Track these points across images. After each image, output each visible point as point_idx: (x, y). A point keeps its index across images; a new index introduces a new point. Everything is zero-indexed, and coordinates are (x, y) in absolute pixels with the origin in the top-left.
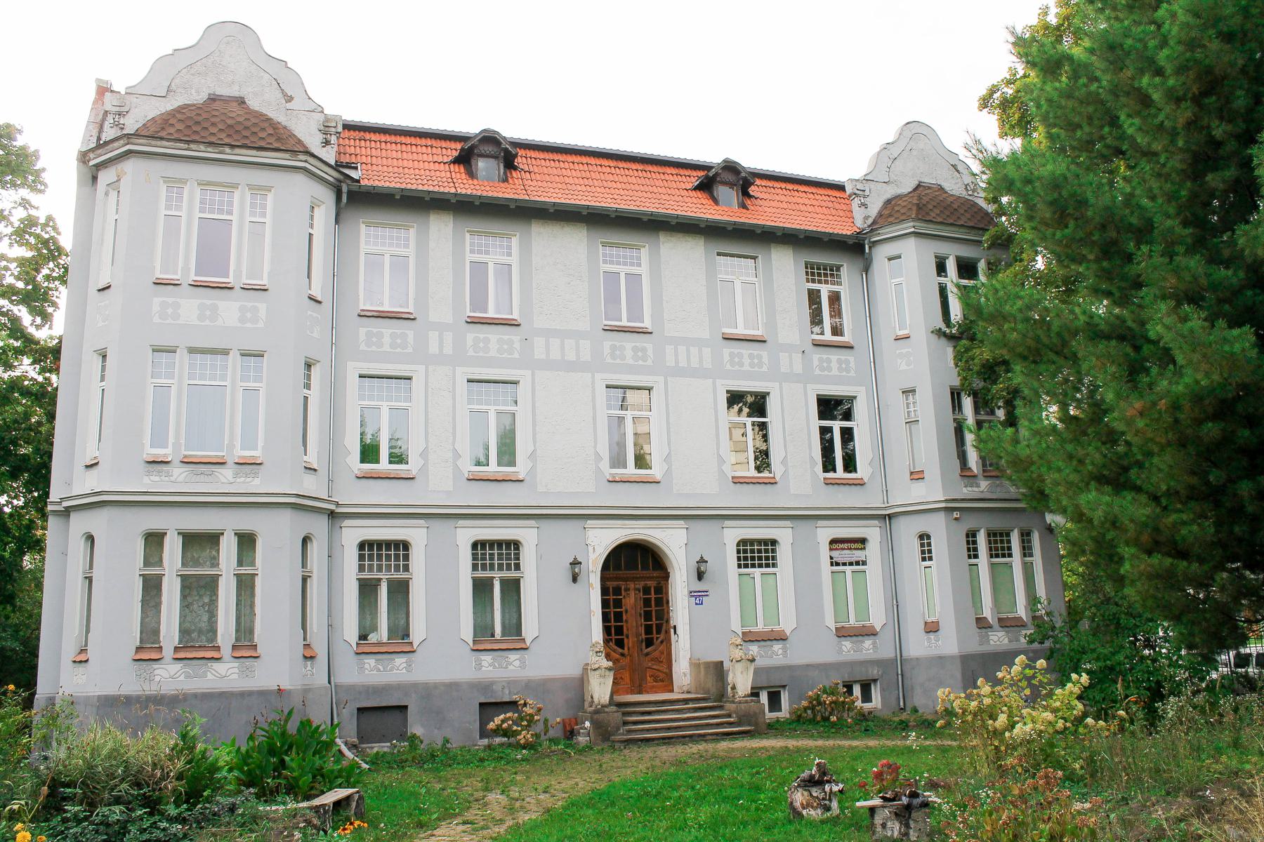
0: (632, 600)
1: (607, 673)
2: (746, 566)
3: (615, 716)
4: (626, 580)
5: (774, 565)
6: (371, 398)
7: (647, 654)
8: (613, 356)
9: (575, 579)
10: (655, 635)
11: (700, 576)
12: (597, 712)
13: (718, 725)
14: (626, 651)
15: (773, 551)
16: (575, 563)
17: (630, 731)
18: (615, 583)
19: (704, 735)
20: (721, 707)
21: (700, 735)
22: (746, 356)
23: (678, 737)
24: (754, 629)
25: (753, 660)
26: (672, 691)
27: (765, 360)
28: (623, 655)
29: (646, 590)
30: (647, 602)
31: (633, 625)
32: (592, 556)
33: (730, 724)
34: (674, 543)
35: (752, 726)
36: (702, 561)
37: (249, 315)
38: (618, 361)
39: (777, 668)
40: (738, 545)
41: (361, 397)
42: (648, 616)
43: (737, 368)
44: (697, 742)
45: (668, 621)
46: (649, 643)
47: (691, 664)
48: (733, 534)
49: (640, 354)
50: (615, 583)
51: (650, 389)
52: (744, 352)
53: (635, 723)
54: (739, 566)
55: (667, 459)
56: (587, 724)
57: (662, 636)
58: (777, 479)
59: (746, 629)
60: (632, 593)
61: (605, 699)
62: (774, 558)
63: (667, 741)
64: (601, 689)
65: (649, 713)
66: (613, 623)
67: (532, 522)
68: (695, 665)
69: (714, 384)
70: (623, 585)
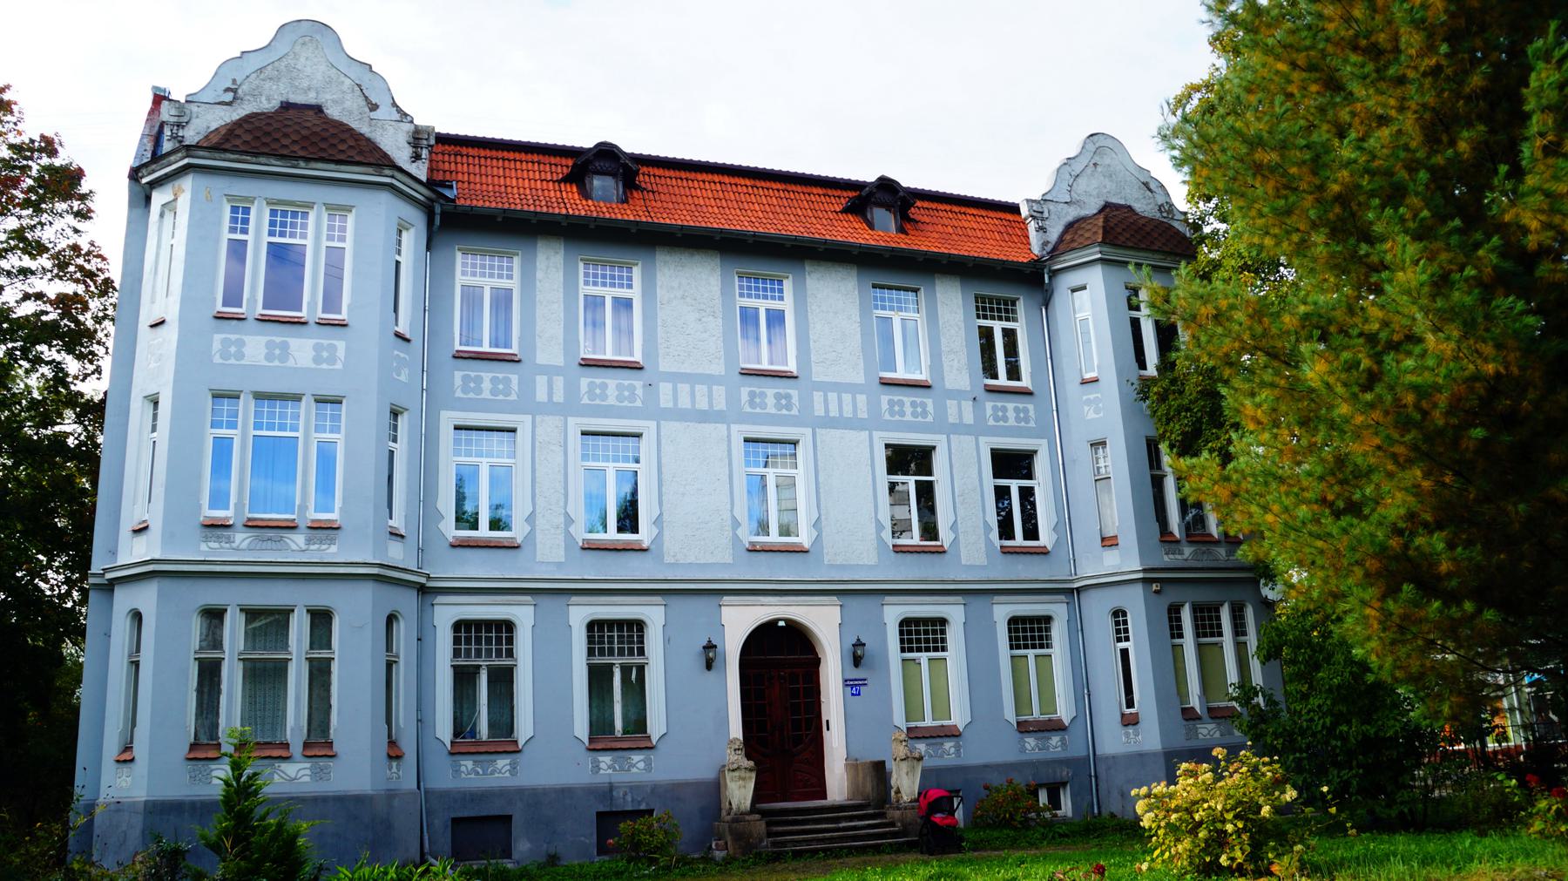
5: (944, 649)
6: (596, 458)
8: (892, 413)
11: (857, 661)
12: (736, 820)
20: (882, 815)
27: (930, 408)
34: (824, 623)
36: (859, 644)
37: (325, 354)
38: (758, 410)
40: (901, 624)
43: (897, 418)
48: (893, 613)
54: (903, 650)
55: (817, 525)
64: (740, 792)
67: (658, 599)
68: (853, 765)
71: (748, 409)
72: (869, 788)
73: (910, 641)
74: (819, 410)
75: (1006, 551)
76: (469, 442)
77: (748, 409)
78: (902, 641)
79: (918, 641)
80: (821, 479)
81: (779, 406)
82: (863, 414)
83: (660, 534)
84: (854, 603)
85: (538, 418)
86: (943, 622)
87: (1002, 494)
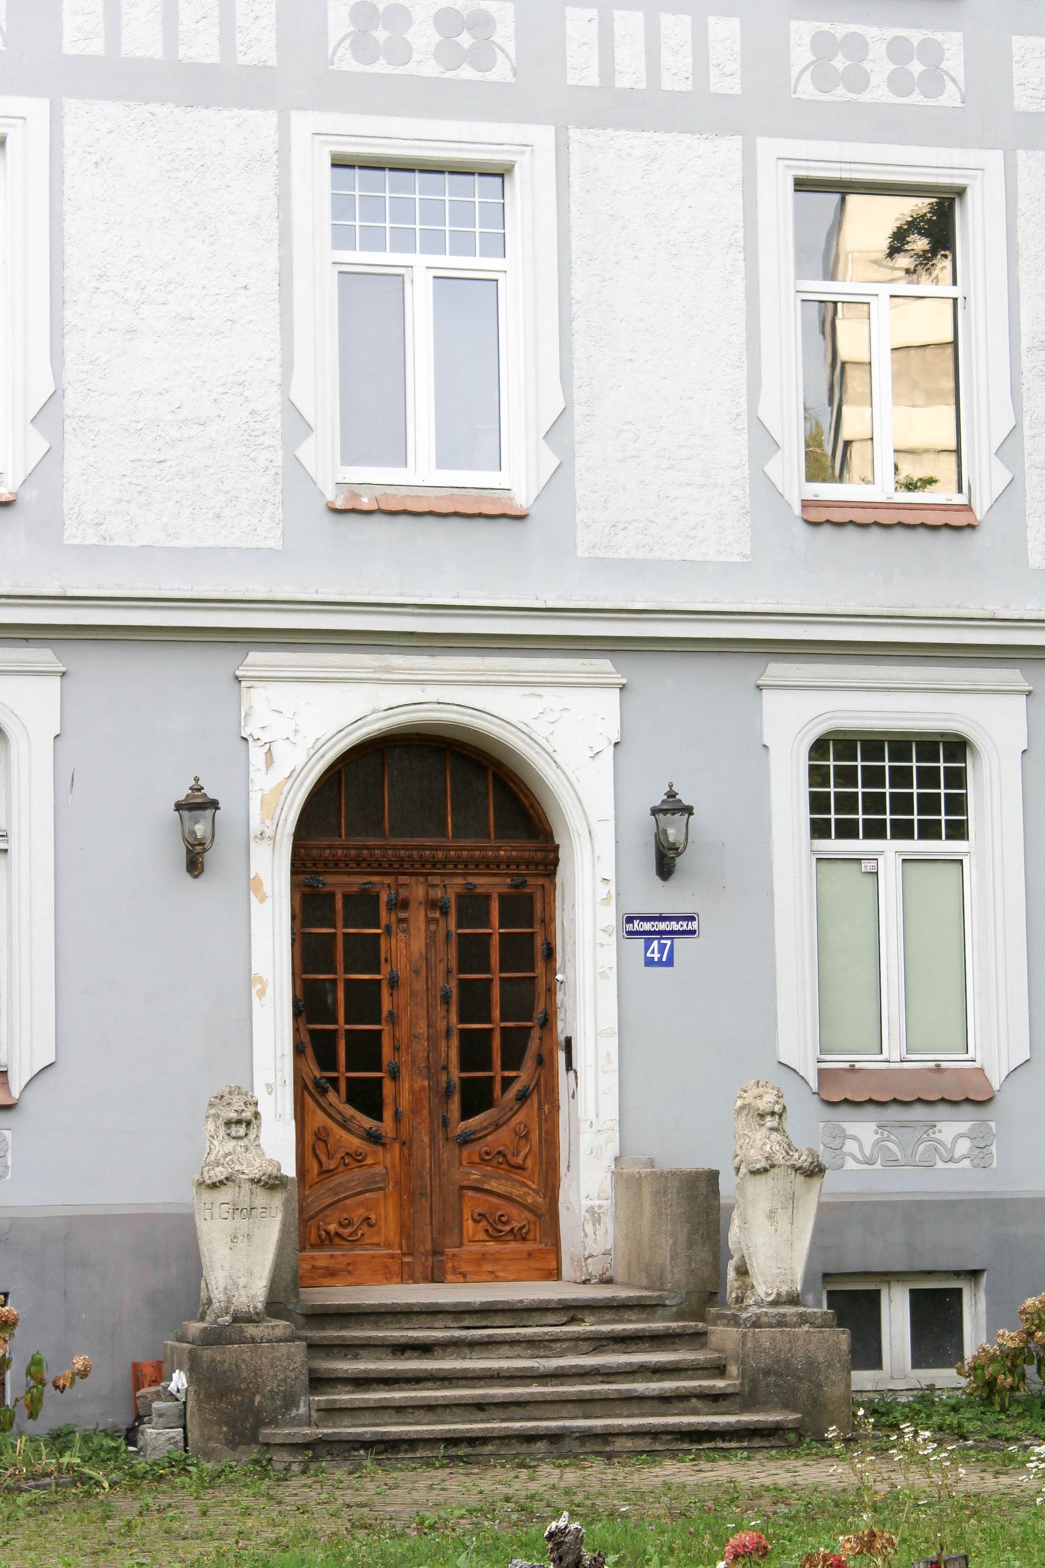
0: (418, 943)
1: (261, 1198)
2: (847, 830)
3: (279, 1356)
4: (396, 868)
5: (958, 831)
6: (373, 241)
7: (465, 1140)
8: (824, 78)
9: (195, 864)
10: (498, 1073)
11: (666, 862)
12: (215, 1337)
13: (666, 1401)
14: (387, 1126)
15: (957, 778)
16: (197, 804)
17: (331, 1411)
18: (355, 882)
19: (606, 1436)
20: (697, 1338)
21: (587, 1436)
22: (878, 50)
23: (506, 1438)
24: (868, 1062)
25: (814, 1171)
26: (555, 1274)
27: (954, 62)
28: (374, 1138)
29: (472, 907)
30: (472, 952)
31: (419, 1031)
32: (263, 782)
33: (715, 1399)
34: (568, 735)
35: (787, 1412)
36: (672, 807)
37: (916, 68)
38: (381, 67)
39: (949, 1208)
40: (819, 748)
41: (342, 238)
42: (473, 1001)
43: (840, 93)
44: (575, 1459)
45: (548, 1022)
46: (476, 1098)
47: (618, 1177)
48: (795, 714)
49: (465, 40)
50: (355, 882)
51: (502, 175)
52: (870, 32)
53: (362, 1382)
54: (819, 830)
55: (558, 432)
56: (179, 1380)
57: (524, 1076)
58: (980, 510)
59: (837, 1061)
60: (418, 917)
61: (254, 1290)
62: (958, 804)
63: (463, 1450)
64: (241, 1261)
65: (425, 1349)
66: (342, 1025)
67: (42, 656)
68: (627, 1181)
69: (749, 155)
70: (384, 888)
71: (347, 63)
72: (663, 1256)
73: (847, 803)
74: (582, 68)
75: (819, 518)
76: (374, 207)
77: (347, 63)
78: (818, 803)
79: (874, 803)
80: (578, 289)
81: (448, 53)
82: (726, 82)
83: (53, 457)
84: (668, 682)
85: (71, 105)
86: (957, 747)
87: (369, 301)
